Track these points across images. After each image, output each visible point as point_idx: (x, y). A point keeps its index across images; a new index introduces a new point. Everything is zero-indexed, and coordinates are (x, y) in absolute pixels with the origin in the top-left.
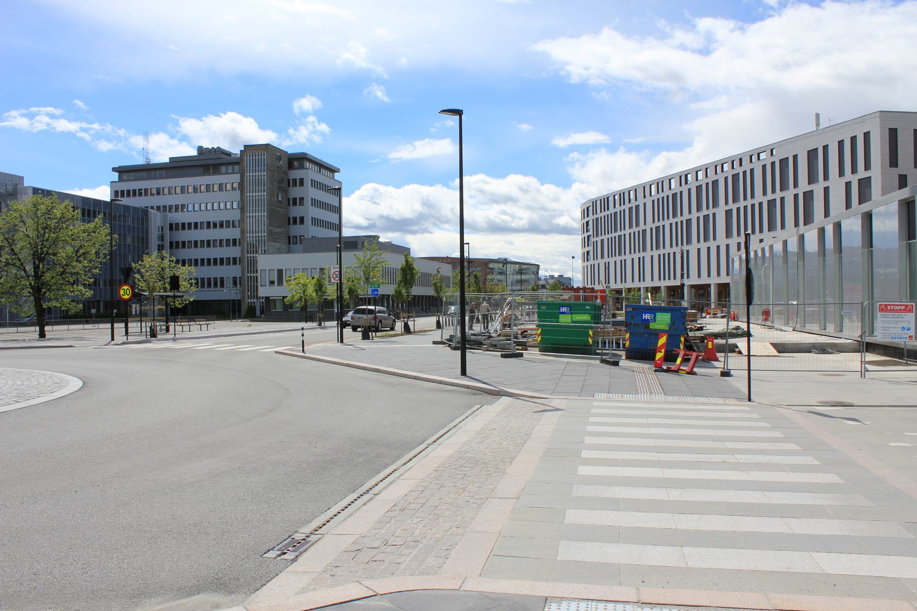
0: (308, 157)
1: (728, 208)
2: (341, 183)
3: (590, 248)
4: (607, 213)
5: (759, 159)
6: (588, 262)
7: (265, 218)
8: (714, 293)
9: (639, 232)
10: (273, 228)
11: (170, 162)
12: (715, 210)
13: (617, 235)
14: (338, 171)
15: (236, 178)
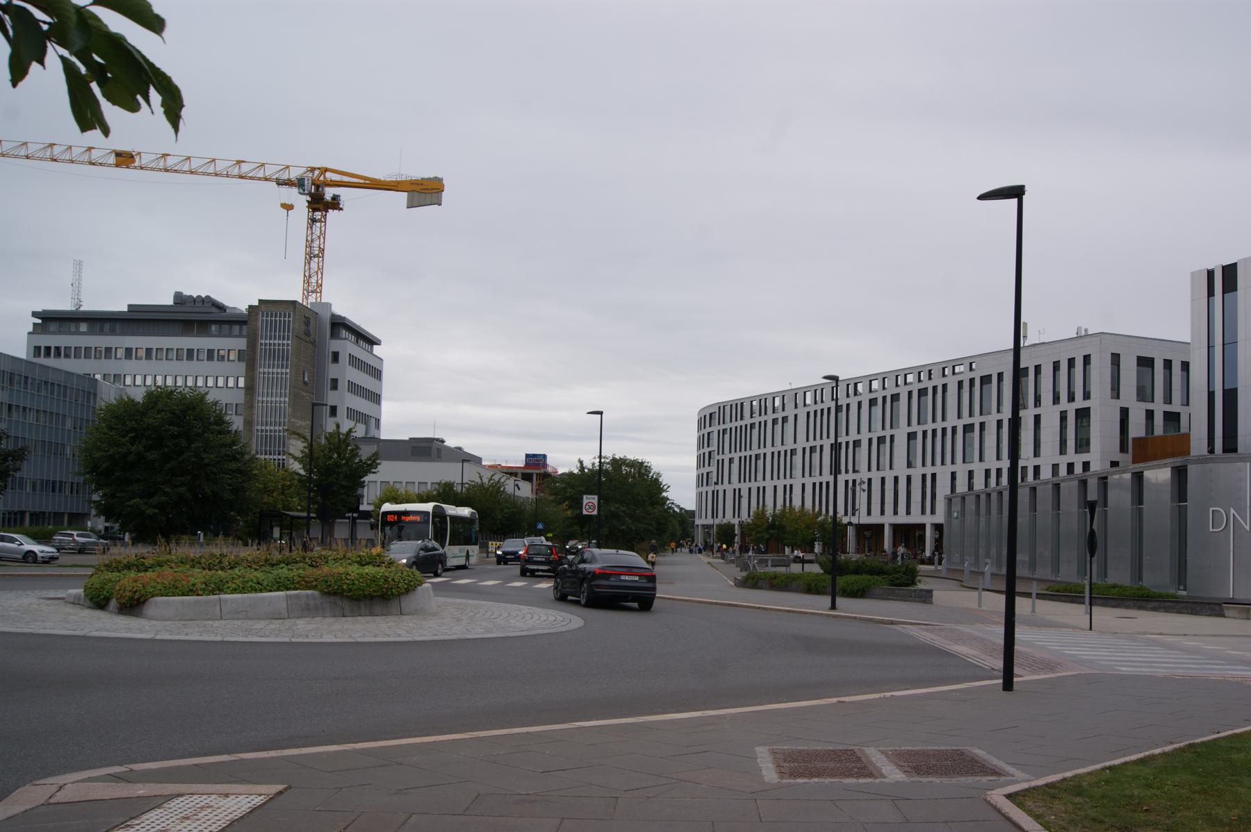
0: (347, 323)
1: (911, 430)
2: (382, 360)
3: (713, 469)
4: (739, 423)
5: (954, 373)
6: (708, 487)
7: (287, 405)
8: (889, 536)
9: (786, 451)
10: (296, 420)
11: (129, 311)
12: (893, 432)
13: (753, 453)
14: (377, 342)
15: (241, 343)
